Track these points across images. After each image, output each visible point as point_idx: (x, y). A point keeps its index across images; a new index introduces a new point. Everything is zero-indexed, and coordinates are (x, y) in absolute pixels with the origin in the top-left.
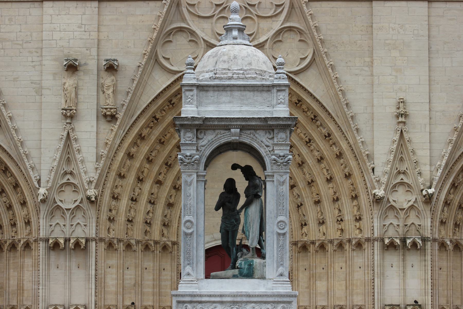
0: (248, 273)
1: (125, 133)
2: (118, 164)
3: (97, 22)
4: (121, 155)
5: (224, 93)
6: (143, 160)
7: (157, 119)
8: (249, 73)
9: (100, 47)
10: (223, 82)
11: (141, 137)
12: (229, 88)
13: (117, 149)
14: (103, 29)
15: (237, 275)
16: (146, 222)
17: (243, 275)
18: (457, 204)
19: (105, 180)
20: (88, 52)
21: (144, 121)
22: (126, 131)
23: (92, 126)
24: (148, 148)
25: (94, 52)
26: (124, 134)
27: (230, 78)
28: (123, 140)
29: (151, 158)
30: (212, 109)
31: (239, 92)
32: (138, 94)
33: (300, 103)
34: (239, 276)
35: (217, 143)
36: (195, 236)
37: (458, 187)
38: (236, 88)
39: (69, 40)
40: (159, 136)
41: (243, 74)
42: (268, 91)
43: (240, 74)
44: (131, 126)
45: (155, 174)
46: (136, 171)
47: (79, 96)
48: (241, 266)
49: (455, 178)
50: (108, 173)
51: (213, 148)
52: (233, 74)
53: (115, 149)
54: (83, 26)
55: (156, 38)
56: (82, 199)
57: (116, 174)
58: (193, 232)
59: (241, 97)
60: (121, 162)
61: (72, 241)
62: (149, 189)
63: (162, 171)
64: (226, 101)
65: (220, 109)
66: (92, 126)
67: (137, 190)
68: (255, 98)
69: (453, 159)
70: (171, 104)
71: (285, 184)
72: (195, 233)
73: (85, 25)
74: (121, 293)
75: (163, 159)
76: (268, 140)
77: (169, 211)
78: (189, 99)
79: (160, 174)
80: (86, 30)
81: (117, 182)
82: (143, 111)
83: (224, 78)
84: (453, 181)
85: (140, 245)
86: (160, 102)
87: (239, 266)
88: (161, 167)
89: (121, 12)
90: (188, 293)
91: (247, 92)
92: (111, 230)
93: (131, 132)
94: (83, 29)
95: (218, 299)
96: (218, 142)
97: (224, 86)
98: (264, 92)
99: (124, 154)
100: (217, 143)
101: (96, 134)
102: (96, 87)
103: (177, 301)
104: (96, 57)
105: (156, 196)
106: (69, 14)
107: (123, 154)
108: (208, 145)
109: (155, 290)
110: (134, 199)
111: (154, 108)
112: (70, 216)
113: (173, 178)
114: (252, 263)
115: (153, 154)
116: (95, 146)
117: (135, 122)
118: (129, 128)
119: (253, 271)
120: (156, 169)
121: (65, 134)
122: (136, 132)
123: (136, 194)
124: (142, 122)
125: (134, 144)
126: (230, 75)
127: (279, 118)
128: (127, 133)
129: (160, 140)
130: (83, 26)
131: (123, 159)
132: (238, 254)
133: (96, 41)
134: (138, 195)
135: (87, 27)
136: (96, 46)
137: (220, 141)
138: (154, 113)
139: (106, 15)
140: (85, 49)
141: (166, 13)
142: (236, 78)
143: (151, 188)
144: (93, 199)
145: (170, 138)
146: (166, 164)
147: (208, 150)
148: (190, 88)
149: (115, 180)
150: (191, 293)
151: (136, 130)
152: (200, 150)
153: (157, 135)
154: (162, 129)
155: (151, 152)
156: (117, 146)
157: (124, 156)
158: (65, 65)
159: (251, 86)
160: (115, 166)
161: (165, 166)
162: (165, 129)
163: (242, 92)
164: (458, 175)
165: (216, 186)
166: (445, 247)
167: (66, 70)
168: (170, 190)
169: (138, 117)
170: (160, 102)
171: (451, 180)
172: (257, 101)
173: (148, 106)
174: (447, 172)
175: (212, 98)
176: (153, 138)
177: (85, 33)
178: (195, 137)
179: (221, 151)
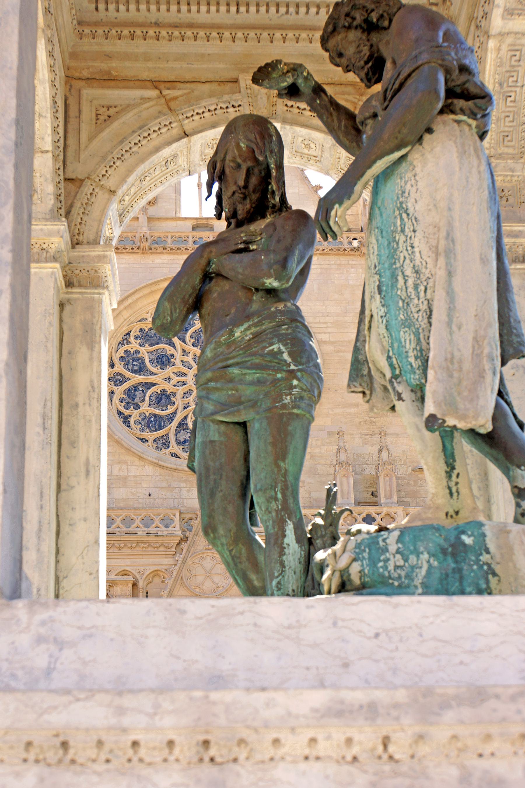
87: (355, 569)
114: (467, 540)
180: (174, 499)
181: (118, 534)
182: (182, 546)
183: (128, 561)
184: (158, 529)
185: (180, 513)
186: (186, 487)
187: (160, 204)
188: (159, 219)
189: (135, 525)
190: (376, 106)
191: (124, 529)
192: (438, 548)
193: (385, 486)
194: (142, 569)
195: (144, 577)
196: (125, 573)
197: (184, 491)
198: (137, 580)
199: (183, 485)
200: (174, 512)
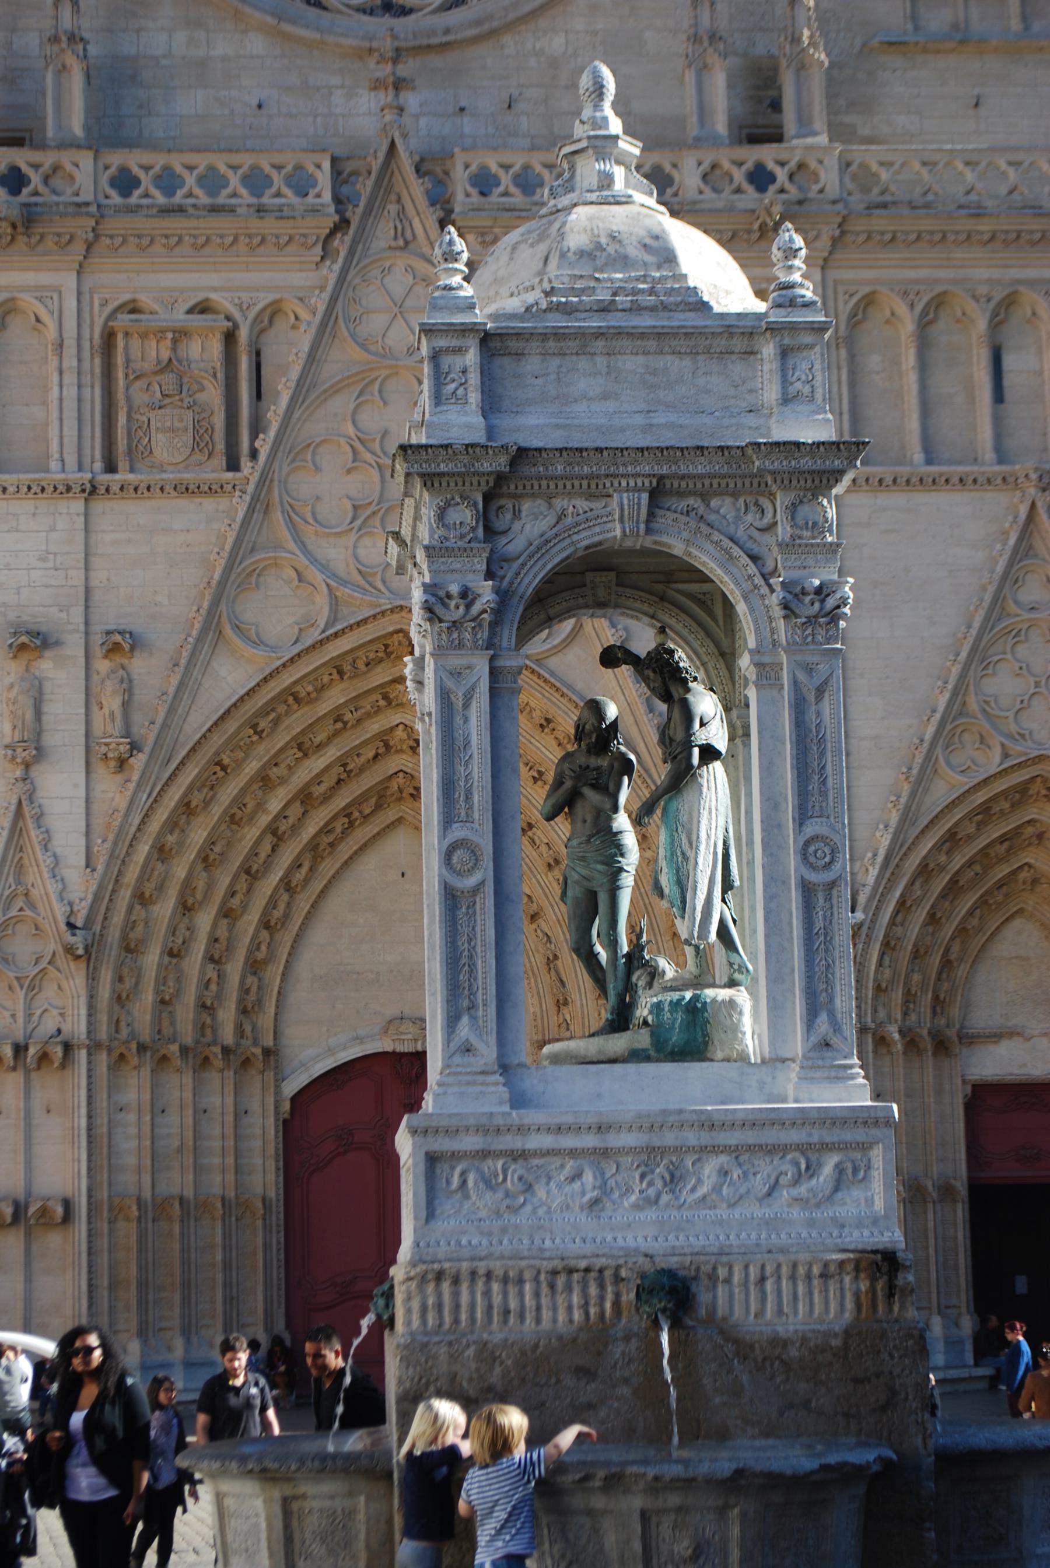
0: (687, 1042)
1: (151, 800)
2: (138, 870)
3: (82, 548)
4: (144, 849)
5: (583, 363)
6: (193, 862)
7: (224, 768)
8: (673, 289)
9: (91, 604)
10: (577, 320)
11: (187, 809)
12: (600, 343)
13: (134, 837)
14: (96, 562)
15: (644, 1050)
16: (204, 1006)
17: (669, 1049)
18: (910, 947)
19: (108, 909)
20: (64, 615)
21: (197, 771)
22: (154, 794)
23: (76, 786)
24: (205, 834)
25: (77, 615)
26: (149, 803)
27: (605, 308)
28: (146, 815)
29: (212, 857)
30: (541, 421)
31: (641, 359)
32: (180, 711)
33: (551, 726)
34: (652, 1053)
35: (564, 549)
36: (490, 902)
37: (914, 908)
38: (626, 343)
39: (19, 589)
40: (230, 806)
41: (652, 292)
42: (745, 353)
43: (641, 291)
44: (167, 784)
45: (222, 893)
46: (178, 887)
47: (45, 718)
48: (658, 1015)
49: (905, 888)
50: (113, 891)
51: (549, 566)
52: (615, 294)
53: (130, 836)
54: (51, 557)
55: (219, 583)
56: (54, 953)
57: (134, 895)
58: (483, 883)
59: (647, 377)
60: (144, 867)
61: (32, 1051)
62: (208, 929)
63: (237, 888)
64: (591, 394)
65: (569, 422)
66: (76, 786)
67: (182, 933)
68: (701, 381)
69: (901, 846)
70: (256, 733)
71: (827, 695)
72: (489, 888)
73: (55, 554)
74: (149, 1168)
75: (241, 859)
76: (756, 534)
77: (256, 980)
78: (453, 386)
79: (233, 894)
80: (58, 565)
81: (135, 913)
82: (193, 750)
83: (581, 308)
84: (902, 895)
85: (191, 1056)
86: (231, 726)
88: (236, 877)
89: (138, 525)
90: (471, 1121)
91: (669, 357)
92: (123, 1024)
93: (166, 797)
94: (50, 564)
95: (589, 1141)
96: (567, 542)
97: (584, 334)
98: (734, 357)
99: (152, 847)
100: (564, 549)
101: (84, 805)
102: (83, 696)
103: (427, 1153)
104: (82, 628)
105: (225, 943)
106: (17, 530)
107: (147, 848)
108: (531, 557)
109: (227, 1160)
110: (175, 951)
111: (217, 740)
112: (26, 995)
113: (264, 903)
115: (217, 849)
116: (84, 829)
117: (174, 774)
118: (162, 789)
119: (705, 1035)
120: (224, 881)
121: (14, 801)
122: (177, 797)
123: (180, 941)
124: (191, 773)
125: (171, 825)
126: (604, 296)
127: (798, 445)
128: (155, 801)
129: (233, 816)
130: (51, 557)
131: (147, 859)
132: (634, 978)
133: (82, 590)
134: (184, 943)
135: (59, 559)
136: (82, 602)
137: (575, 538)
138: (217, 753)
139: (103, 531)
140: (56, 608)
141: (241, 527)
142: (628, 305)
143: (215, 926)
144: (81, 952)
145: (255, 812)
146: (248, 872)
147: (531, 575)
148: (455, 343)
149: (130, 909)
150: (484, 1120)
151: (175, 795)
152: (501, 573)
153: (227, 803)
154: (236, 791)
155: (213, 843)
156: (133, 829)
157: (149, 853)
158: (11, 645)
159: (686, 334)
160: (132, 875)
161: (244, 877)
162: (243, 791)
163: (651, 357)
164: (913, 883)
165: (361, 921)
166: (888, 1045)
167: (15, 657)
168: (257, 932)
169: (182, 763)
170: (231, 726)
171: (898, 894)
172: (708, 392)
173: (204, 736)
174: (888, 875)
175: (540, 381)
176: (217, 811)
177: (53, 572)
178: (481, 524)
179: (551, 612)
180: (315, 117)
181: (191, 211)
182: (336, 243)
183: (213, 279)
184: (283, 201)
185: (334, 160)
186: (342, 87)
187: (827, 190)
188: (995, 1036)
189: (229, 190)
190: (254, 1397)
191: (204, 199)
192: (709, 1055)
193: (409, 1311)
194: (245, 297)
195: (251, 315)
196: (203, 308)
197: (338, 98)
198: (236, 326)
199: (336, 80)
200: (317, 157)
